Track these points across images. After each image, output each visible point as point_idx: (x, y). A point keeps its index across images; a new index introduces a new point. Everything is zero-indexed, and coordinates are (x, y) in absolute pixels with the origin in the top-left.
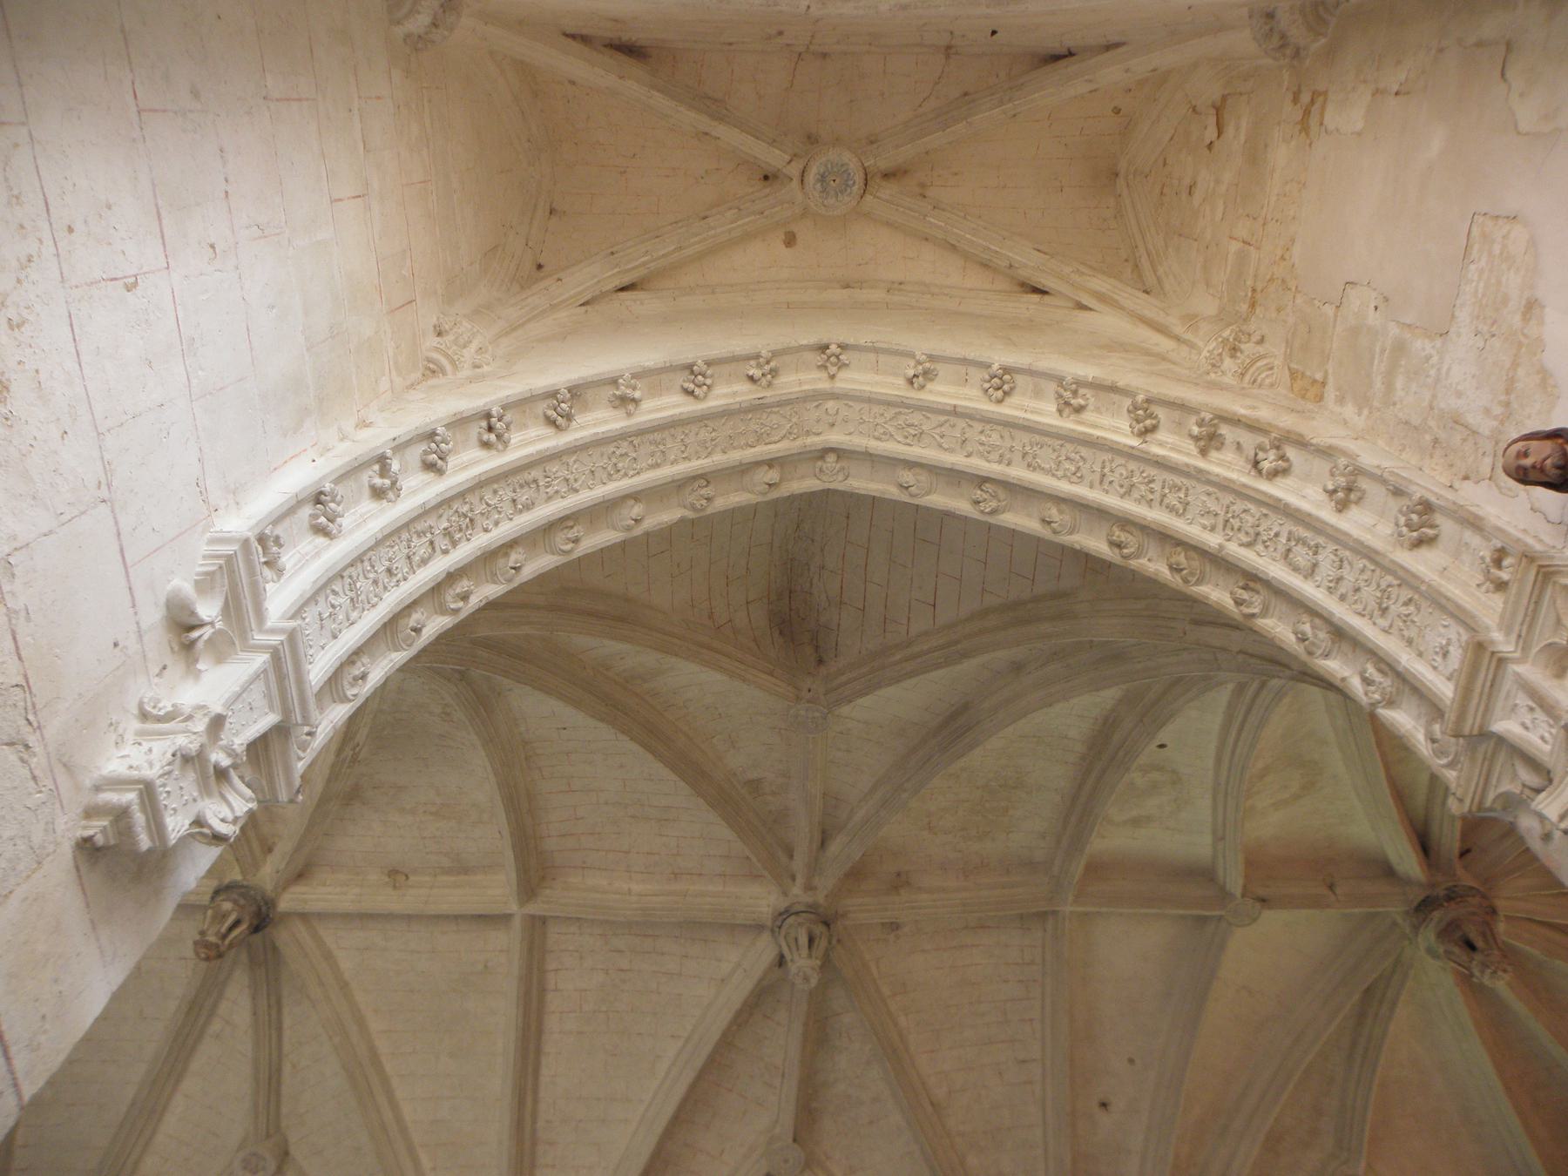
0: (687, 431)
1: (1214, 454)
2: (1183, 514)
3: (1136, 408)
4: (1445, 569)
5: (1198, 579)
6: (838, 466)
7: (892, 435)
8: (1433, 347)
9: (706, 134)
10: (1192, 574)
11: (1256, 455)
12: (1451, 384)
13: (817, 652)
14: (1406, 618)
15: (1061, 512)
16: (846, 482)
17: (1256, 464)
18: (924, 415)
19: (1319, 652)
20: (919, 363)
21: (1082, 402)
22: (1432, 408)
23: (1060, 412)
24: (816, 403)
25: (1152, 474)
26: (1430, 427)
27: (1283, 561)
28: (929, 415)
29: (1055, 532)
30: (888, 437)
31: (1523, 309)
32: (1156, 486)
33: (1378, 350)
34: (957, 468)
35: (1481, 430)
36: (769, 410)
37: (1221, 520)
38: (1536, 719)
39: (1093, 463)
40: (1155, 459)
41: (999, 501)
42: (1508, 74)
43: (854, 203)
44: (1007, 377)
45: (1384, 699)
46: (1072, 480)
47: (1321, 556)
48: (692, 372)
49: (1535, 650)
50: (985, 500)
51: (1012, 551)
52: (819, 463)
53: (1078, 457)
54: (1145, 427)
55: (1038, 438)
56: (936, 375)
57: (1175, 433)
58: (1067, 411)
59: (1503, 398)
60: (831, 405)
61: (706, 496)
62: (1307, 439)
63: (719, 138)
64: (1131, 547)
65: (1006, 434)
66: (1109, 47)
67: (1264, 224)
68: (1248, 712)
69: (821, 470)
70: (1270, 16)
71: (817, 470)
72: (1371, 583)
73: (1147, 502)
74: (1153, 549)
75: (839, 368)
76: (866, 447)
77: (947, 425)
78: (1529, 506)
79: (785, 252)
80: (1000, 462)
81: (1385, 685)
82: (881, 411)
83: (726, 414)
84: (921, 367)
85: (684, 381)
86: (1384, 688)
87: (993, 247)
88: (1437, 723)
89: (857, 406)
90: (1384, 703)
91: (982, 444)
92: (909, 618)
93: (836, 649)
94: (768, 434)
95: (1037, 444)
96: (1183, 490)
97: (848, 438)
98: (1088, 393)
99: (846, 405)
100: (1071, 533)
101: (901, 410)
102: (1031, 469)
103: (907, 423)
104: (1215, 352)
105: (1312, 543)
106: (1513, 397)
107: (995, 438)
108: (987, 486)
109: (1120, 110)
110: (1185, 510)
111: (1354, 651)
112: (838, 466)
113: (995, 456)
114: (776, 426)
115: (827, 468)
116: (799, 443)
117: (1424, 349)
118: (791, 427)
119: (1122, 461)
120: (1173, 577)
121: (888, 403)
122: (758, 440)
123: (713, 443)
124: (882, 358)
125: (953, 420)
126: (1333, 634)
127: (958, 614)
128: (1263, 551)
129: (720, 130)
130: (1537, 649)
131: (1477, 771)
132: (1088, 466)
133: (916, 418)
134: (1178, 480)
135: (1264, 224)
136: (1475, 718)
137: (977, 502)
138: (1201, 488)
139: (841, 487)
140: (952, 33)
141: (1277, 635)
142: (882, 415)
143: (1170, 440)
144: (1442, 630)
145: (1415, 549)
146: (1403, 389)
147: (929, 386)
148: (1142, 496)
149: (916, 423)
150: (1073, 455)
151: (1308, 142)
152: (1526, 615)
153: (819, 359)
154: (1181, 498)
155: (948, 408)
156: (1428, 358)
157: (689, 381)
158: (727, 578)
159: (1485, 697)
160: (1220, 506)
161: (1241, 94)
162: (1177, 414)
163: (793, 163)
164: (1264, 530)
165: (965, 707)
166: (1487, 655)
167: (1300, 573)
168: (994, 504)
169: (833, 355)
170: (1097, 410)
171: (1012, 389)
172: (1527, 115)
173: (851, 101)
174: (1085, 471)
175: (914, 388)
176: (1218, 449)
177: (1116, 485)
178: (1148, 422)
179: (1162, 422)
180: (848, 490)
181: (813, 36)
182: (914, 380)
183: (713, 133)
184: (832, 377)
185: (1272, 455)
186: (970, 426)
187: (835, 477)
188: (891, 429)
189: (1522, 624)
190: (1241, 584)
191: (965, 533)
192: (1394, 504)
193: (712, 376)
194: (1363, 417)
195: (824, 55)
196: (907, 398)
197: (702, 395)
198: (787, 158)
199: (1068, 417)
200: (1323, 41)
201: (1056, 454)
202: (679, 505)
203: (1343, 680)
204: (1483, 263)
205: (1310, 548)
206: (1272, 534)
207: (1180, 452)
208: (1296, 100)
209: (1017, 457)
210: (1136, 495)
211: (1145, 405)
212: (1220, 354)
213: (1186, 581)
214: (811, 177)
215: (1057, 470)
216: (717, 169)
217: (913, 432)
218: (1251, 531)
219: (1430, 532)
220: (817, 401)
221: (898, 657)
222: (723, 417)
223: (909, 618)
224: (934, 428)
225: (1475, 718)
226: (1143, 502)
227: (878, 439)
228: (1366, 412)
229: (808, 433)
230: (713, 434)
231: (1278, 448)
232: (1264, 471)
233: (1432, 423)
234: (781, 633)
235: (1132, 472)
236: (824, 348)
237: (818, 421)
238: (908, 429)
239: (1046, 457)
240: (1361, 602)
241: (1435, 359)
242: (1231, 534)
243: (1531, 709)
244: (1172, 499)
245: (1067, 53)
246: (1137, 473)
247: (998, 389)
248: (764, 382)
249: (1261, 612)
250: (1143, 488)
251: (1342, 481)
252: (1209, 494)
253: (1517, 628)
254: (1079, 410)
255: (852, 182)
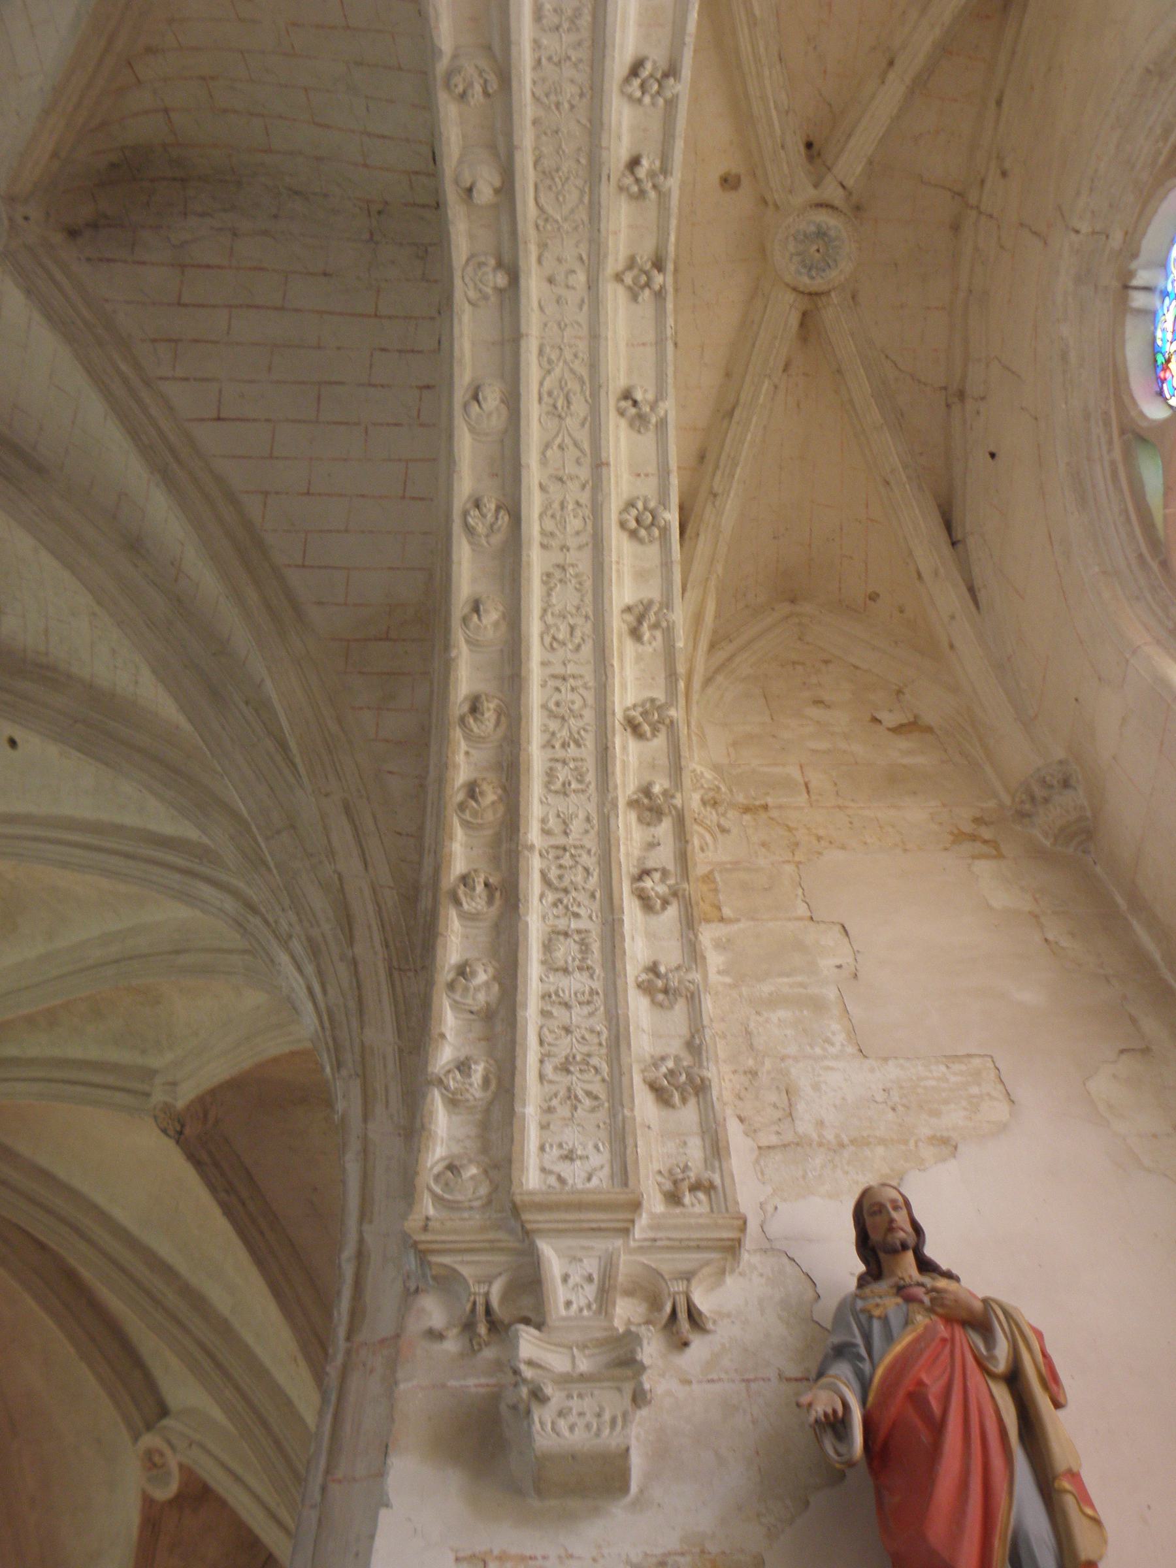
0: (581, 66)
1: (633, 816)
2: (550, 791)
3: (659, 709)
4: (649, 1127)
5: (468, 822)
6: (489, 291)
7: (549, 372)
8: (843, 1045)
9: (891, 63)
10: (475, 814)
11: (656, 870)
12: (819, 1075)
13: (88, 225)
14: (571, 1095)
15: (496, 625)
16: (467, 304)
17: (646, 873)
18: (585, 419)
19: (457, 997)
20: (653, 406)
21: (646, 637)
22: (783, 1059)
23: (629, 609)
24: (585, 257)
25: (587, 743)
26: (763, 1063)
27: (550, 929)
28: (587, 425)
29: (465, 620)
30: (546, 366)
31: (938, 1134)
32: (573, 750)
33: (799, 979)
34: (524, 473)
35: (797, 1122)
36: (587, 190)
37: (561, 840)
38: (582, 1287)
39: (576, 663)
40: (609, 744)
41: (487, 536)
42: (1124, 1057)
43: (788, 278)
44: (656, 532)
45: (453, 1093)
46: (545, 637)
47: (578, 974)
48: (666, 75)
49: (644, 1259)
50: (484, 516)
51: (338, 531)
52: (492, 262)
53: (577, 641)
54: (639, 725)
55: (588, 584)
56: (639, 432)
57: (641, 763)
58: (630, 618)
59: (846, 1140)
60: (581, 278)
61: (470, 92)
62: (700, 929)
63: (883, 82)
64: (478, 728)
65: (585, 538)
66: (971, 590)
67: (839, 807)
68: (127, 856)
69: (480, 265)
70: (1066, 784)
71: (483, 259)
72: (584, 1044)
73: (549, 742)
74: (484, 755)
75: (630, 289)
76: (527, 335)
77: (578, 454)
78: (762, 1200)
79: (714, 178)
80: (543, 533)
81: (472, 1090)
82: (581, 355)
83: (595, 127)
84: (648, 409)
85: (654, 62)
86: (467, 1090)
87: (739, 470)
88: (478, 1168)
89: (582, 317)
90: (450, 1096)
91: (562, 506)
92: (186, 379)
93: (101, 260)
94: (550, 188)
95: (580, 584)
96: (580, 787)
97: (535, 305)
98: (658, 643)
99: (583, 301)
100: (468, 642)
101: (588, 385)
102: (544, 578)
103: (571, 395)
104: (703, 781)
105: (589, 962)
106: (852, 1148)
107: (575, 524)
108: (504, 519)
109: (874, 601)
110: (556, 792)
111: (479, 1040)
112: (489, 291)
113: (550, 525)
114: (561, 199)
115: (484, 274)
116: (532, 233)
117: (834, 1034)
118: (557, 221)
119: (590, 700)
120: (459, 789)
121: (594, 365)
122: (544, 173)
123: (553, 107)
124: (650, 351)
125: (587, 461)
126: (487, 1009)
127: (214, 456)
128: (547, 901)
129: (895, 88)
130: (646, 1262)
131: (473, 1238)
132: (570, 656)
133: (580, 408)
134: (590, 777)
135: (839, 807)
136: (546, 1222)
137: (477, 505)
138: (592, 808)
139: (458, 295)
140: (983, 399)
141: (448, 938)
142: (576, 356)
143: (631, 758)
144: (590, 1146)
145: (647, 1087)
146: (779, 1019)
147: (623, 423)
148: (553, 734)
149: (572, 407)
150: (578, 633)
151: (948, 845)
152: (681, 1240)
153: (644, 258)
154: (570, 784)
155: (604, 455)
156: (828, 1041)
157: (655, 68)
158: (212, 78)
159: (577, 1225)
160: (578, 836)
161: (946, 751)
162: (663, 761)
163: (840, 190)
164: (574, 899)
165: (40, 469)
166: (629, 1216)
167: (544, 954)
168: (481, 529)
169: (649, 279)
170: (639, 658)
171: (641, 541)
172: (1102, 1086)
173: (896, 265)
174: (561, 652)
175: (618, 400)
176: (640, 820)
177: (556, 697)
178: (646, 728)
179: (649, 744)
180: (456, 308)
181: (991, 216)
182: (630, 402)
183: (891, 76)
184: (619, 278)
185: (662, 889)
186: (583, 487)
187: (471, 285)
188: (557, 371)
189: (669, 1239)
190: (491, 880)
191: (345, 460)
192: (675, 1047)
193: (653, 104)
194: (721, 978)
195: (956, 228)
196: (607, 393)
197: (629, 90)
198: (850, 183)
199: (624, 621)
200: (1048, 843)
201: (574, 611)
202: (457, 48)
203: (443, 1036)
204: (953, 1079)
205: (583, 959)
206: (575, 909)
207: (624, 774)
208: (977, 821)
209: (558, 558)
210: (553, 725)
211: (667, 721)
212: (702, 787)
213: (462, 807)
214: (824, 218)
215: (553, 614)
216: (825, 72)
217: (559, 404)
218: (566, 883)
219: (676, 1097)
220: (589, 259)
221: (124, 367)
222: (590, 121)
223: (186, 379)
224: (570, 435)
225: (546, 1222)
226: (547, 736)
227: (541, 352)
228: (728, 980)
229: (543, 246)
230: (566, 106)
231: (675, 894)
232: (642, 884)
233: (768, 1064)
234: (113, 165)
235: (581, 716)
236: (659, 265)
237: (559, 260)
238: (562, 396)
239: (566, 598)
240: (556, 1039)
241: (832, 1050)
242: (550, 857)
243: (590, 1279)
244: (563, 774)
245: (954, 540)
246: (581, 723)
247: (637, 521)
248: (628, 180)
249: (465, 912)
250: (565, 733)
251: (674, 983)
252: (588, 819)
253: (660, 1235)
254: (635, 634)
255: (814, 275)
